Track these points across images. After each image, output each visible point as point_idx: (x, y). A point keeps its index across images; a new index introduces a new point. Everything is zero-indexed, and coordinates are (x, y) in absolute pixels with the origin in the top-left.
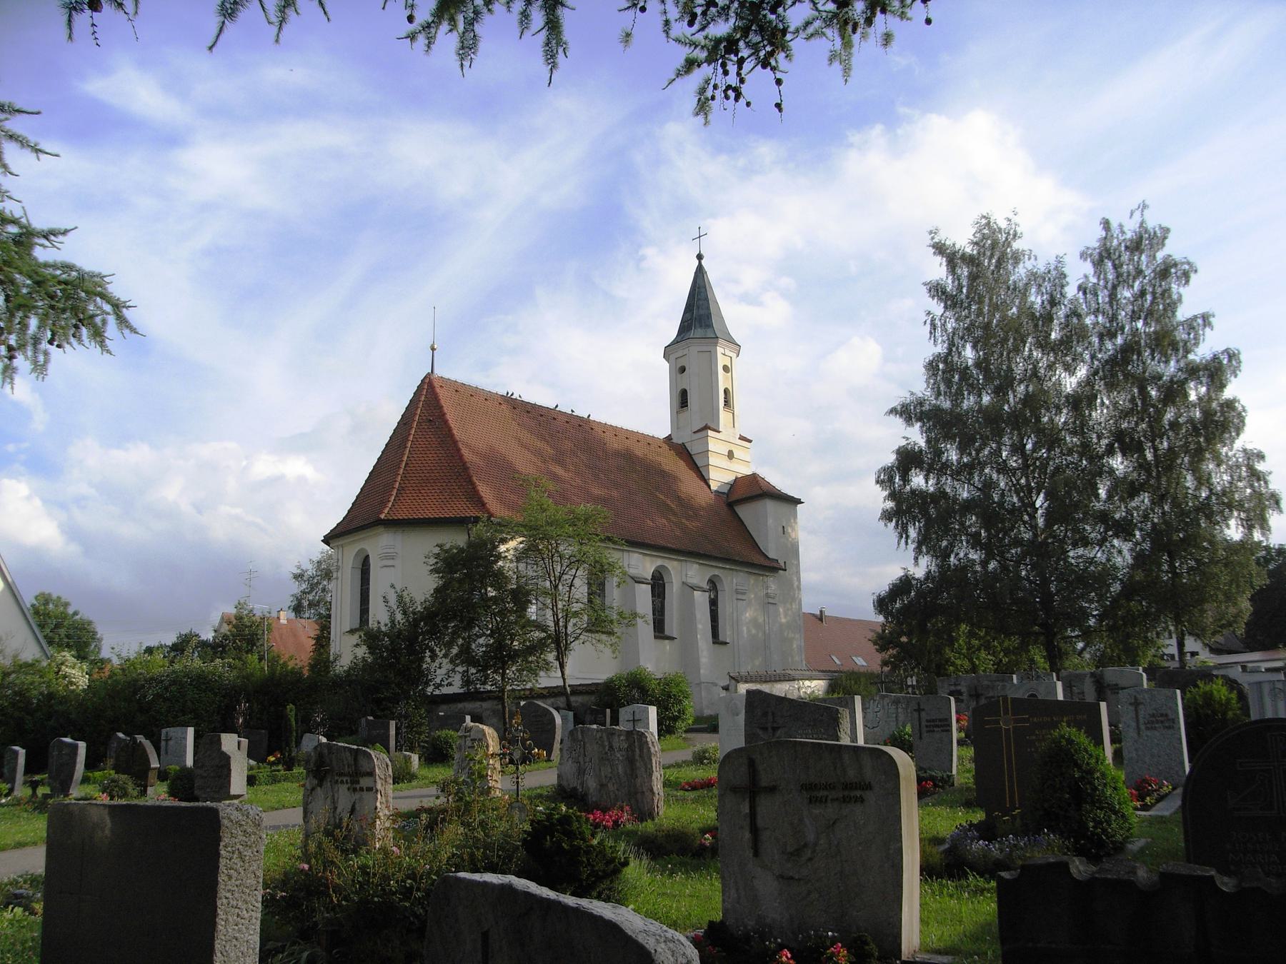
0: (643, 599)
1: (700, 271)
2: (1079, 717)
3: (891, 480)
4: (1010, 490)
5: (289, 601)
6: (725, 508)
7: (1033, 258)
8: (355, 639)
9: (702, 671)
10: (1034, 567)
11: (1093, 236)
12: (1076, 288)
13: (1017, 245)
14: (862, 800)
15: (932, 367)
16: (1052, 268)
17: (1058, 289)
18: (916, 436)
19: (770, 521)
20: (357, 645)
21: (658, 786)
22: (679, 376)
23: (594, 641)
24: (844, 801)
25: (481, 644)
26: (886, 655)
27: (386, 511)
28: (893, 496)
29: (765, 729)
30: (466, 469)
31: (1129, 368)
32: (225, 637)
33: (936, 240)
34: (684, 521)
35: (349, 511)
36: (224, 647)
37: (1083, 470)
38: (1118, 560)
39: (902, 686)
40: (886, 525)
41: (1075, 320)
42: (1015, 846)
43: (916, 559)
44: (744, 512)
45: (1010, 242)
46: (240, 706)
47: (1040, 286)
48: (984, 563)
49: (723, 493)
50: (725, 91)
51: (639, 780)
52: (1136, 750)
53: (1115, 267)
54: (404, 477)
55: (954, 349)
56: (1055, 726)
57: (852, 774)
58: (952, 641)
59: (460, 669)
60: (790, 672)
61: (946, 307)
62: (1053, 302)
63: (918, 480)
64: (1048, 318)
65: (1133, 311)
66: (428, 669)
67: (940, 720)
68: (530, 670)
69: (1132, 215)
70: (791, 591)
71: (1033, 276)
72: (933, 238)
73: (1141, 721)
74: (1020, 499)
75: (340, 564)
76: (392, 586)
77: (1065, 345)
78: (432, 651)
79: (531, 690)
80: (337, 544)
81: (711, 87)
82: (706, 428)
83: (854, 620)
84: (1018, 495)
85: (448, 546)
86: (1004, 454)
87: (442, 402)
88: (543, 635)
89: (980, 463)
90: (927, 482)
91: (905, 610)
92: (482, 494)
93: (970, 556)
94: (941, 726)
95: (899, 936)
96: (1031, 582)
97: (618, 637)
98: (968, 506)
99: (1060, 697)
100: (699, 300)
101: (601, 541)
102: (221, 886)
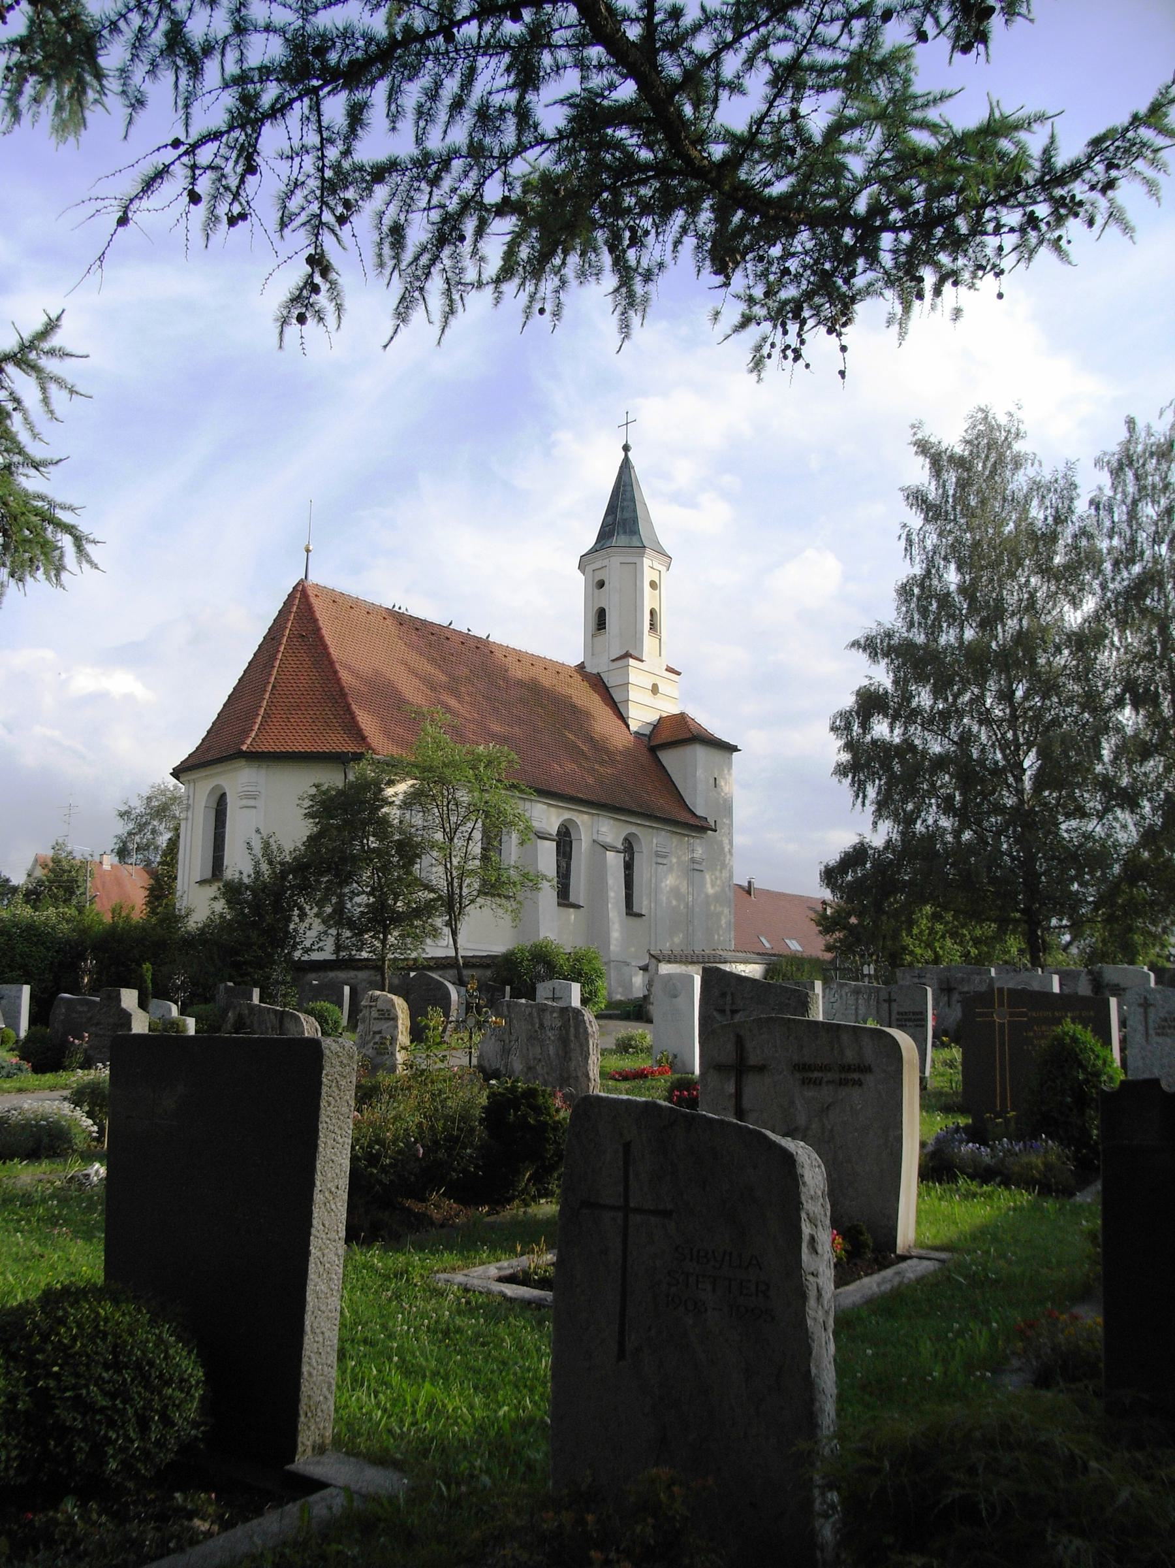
0: (546, 857)
1: (626, 466)
2: (1084, 1014)
3: (848, 727)
4: (993, 745)
5: (112, 844)
6: (645, 751)
7: (1036, 463)
8: (212, 890)
9: (612, 948)
10: (1018, 840)
11: (1113, 441)
12: (1087, 503)
13: (1018, 446)
14: (859, 1083)
15: (904, 591)
16: (1059, 476)
17: (1067, 503)
18: (882, 676)
19: (699, 773)
20: (215, 898)
21: (594, 1071)
22: (596, 591)
23: (494, 906)
24: (840, 1084)
25: (360, 903)
26: (830, 939)
27: (248, 742)
28: (850, 746)
29: (722, 1011)
30: (344, 695)
31: (1148, 602)
32: (40, 883)
33: (919, 436)
34: (597, 767)
35: (203, 740)
36: (38, 894)
37: (1084, 725)
38: (1122, 837)
39: (858, 975)
40: (840, 781)
41: (1084, 542)
42: (1009, 1151)
43: (875, 824)
44: (669, 759)
45: (1010, 443)
46: (86, 962)
47: (1043, 497)
48: (957, 833)
49: (645, 735)
50: (784, 351)
51: (573, 1065)
52: (1143, 1058)
53: (1137, 478)
54: (271, 703)
55: (933, 571)
56: (1059, 1021)
57: (850, 1056)
58: (911, 923)
59: (333, 931)
60: (721, 953)
61: (926, 519)
62: (1058, 520)
63: (881, 729)
64: (1052, 538)
65: (1156, 532)
66: (295, 930)
67: (914, 1013)
68: (416, 937)
69: (1161, 414)
70: (719, 858)
71: (1036, 486)
72: (915, 434)
73: (1151, 1025)
74: (1005, 757)
75: (191, 802)
76: (258, 831)
77: (1071, 571)
78: (301, 909)
79: (415, 960)
80: (189, 778)
81: (768, 345)
82: (627, 655)
83: (789, 895)
84: (1003, 751)
85: (324, 788)
86: (989, 701)
87: (318, 615)
88: (432, 896)
89: (957, 711)
90: (892, 731)
91: (858, 883)
92: (363, 727)
93: (940, 823)
94: (915, 1020)
95: (894, 1228)
96: (1013, 859)
97: (519, 903)
98: (940, 762)
99: (1056, 989)
100: (624, 500)
101: (506, 789)
102: (322, 1111)
